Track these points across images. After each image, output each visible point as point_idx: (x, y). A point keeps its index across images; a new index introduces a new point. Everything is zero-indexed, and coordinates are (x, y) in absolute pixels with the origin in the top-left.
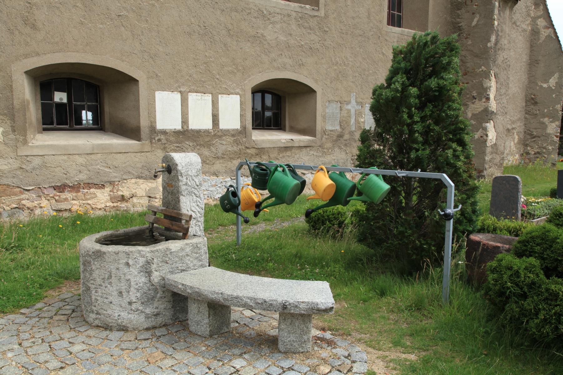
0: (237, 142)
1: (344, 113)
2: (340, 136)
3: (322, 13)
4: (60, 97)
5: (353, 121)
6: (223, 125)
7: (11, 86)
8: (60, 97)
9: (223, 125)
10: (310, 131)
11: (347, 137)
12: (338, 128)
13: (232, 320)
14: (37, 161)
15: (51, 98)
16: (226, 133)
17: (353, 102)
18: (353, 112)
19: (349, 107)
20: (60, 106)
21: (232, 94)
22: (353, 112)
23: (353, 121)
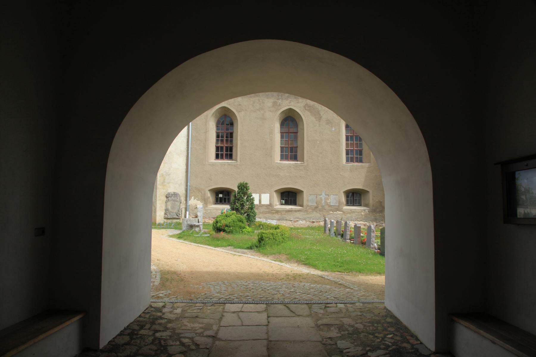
0: (268, 209)
1: (318, 198)
2: (316, 207)
3: (306, 164)
4: (221, 196)
5: (323, 202)
6: (263, 203)
7: (291, 228)
8: (221, 196)
9: (263, 203)
10: (302, 206)
11: (320, 207)
12: (315, 204)
13: (230, 104)
14: (209, 211)
15: (218, 196)
16: (264, 205)
17: (323, 194)
18: (323, 198)
19: (321, 196)
20: (221, 198)
21: (134, 322)
22: (323, 198)
23: (323, 202)
